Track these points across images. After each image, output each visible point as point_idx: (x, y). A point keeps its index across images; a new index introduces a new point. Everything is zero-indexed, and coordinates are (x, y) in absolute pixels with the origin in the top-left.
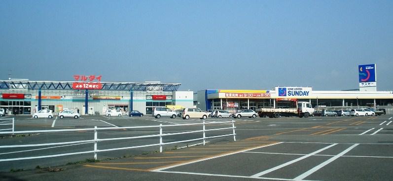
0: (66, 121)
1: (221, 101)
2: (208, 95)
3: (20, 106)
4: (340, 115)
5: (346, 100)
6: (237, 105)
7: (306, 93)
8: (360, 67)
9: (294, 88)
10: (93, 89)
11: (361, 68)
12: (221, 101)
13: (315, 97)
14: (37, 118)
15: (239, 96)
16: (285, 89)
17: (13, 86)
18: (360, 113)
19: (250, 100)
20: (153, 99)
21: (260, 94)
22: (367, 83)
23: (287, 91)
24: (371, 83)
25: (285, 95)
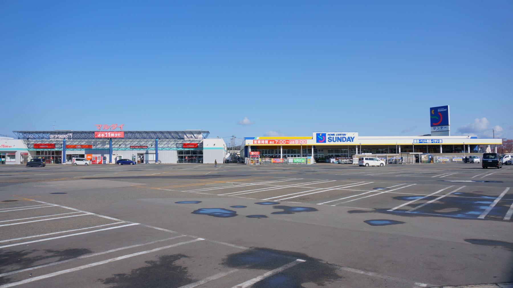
1: (441, 148)
3: (184, 155)
5: (444, 146)
6: (257, 153)
7: (351, 139)
8: (431, 109)
9: (336, 133)
10: (115, 138)
11: (433, 111)
12: (441, 148)
14: (369, 166)
15: (269, 143)
16: (324, 135)
17: (192, 135)
18: (371, 163)
19: (284, 147)
20: (183, 148)
21: (295, 141)
22: (440, 127)
23: (327, 137)
24: (444, 127)
25: (325, 142)
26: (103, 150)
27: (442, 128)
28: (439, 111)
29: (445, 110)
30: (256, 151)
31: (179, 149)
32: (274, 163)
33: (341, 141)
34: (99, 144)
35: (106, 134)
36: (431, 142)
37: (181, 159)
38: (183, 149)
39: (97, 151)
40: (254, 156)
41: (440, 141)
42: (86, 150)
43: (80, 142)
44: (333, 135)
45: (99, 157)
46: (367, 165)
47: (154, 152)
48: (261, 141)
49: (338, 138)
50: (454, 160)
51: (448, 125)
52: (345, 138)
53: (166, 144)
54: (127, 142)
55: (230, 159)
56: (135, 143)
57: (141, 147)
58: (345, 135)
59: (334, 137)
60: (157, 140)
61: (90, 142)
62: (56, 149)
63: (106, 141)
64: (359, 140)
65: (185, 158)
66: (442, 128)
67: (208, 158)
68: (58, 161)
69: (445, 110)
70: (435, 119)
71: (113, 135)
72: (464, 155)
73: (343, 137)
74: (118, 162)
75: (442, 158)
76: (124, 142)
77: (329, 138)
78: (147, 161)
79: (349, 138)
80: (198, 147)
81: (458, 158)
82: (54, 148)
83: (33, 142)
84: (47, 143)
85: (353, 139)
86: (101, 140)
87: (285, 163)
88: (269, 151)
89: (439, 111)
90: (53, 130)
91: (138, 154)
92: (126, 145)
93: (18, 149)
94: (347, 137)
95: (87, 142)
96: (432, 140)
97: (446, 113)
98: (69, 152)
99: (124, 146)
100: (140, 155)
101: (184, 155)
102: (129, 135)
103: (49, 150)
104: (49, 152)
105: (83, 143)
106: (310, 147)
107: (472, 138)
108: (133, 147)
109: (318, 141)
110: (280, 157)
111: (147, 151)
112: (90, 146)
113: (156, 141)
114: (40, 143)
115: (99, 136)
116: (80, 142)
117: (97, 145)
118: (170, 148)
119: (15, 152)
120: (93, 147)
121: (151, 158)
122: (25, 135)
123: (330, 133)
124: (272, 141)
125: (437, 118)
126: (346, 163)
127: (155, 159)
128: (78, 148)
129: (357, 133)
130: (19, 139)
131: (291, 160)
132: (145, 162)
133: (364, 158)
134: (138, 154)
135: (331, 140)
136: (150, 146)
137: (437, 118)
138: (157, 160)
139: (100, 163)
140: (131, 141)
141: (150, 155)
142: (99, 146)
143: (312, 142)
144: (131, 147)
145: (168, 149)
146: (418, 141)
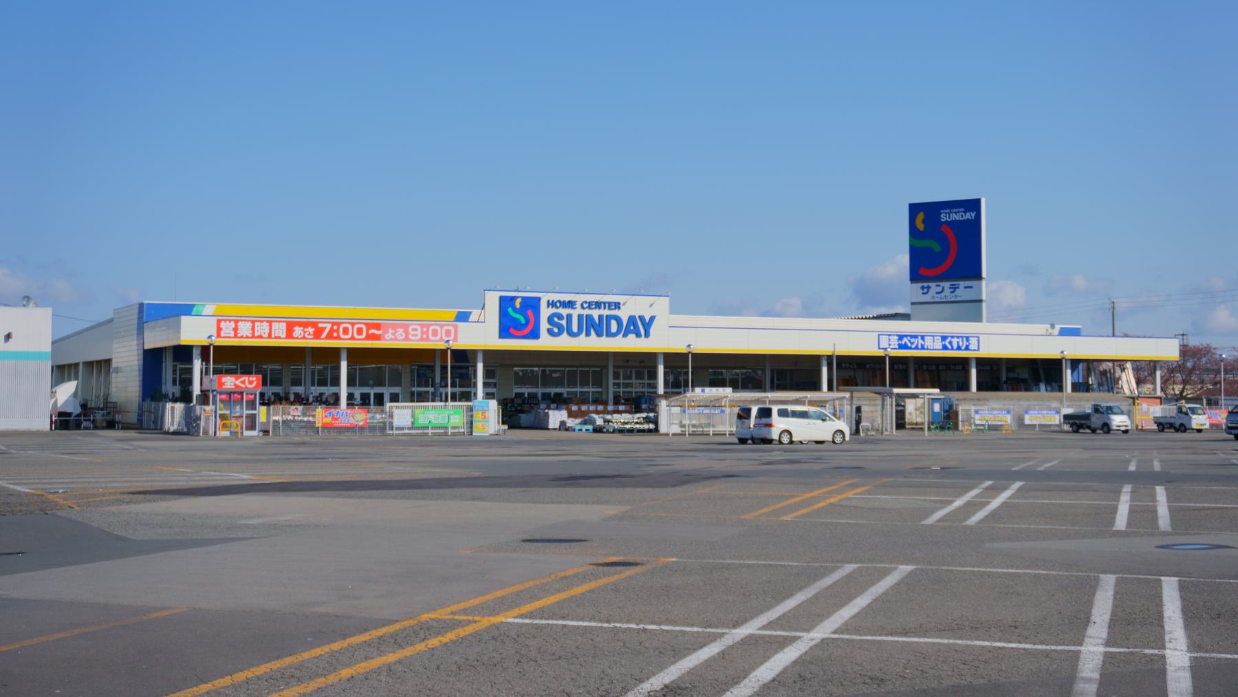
0: (344, 437)
1: (974, 372)
2: (913, 401)
4: (1183, 428)
6: (250, 383)
8: (914, 209)
11: (921, 216)
12: (974, 372)
13: (678, 347)
15: (289, 335)
16: (531, 305)
18: (803, 430)
19: (354, 354)
21: (406, 328)
22: (947, 285)
23: (545, 312)
24: (962, 284)
25: (535, 335)
27: (954, 288)
28: (944, 218)
29: (970, 216)
30: (246, 371)
32: (326, 427)
33: (599, 334)
36: (939, 345)
40: (233, 397)
41: (973, 342)
44: (570, 304)
46: (785, 439)
48: (264, 329)
49: (589, 317)
50: (1028, 420)
51: (978, 276)
52: (618, 320)
55: (75, 409)
58: (617, 306)
59: (575, 313)
64: (674, 334)
66: (954, 288)
68: (641, 402)
69: (970, 216)
70: (929, 249)
72: (1068, 402)
73: (609, 318)
75: (985, 411)
77: (550, 320)
79: (632, 320)
81: (1045, 410)
85: (647, 325)
87: (372, 429)
88: (288, 372)
89: (944, 218)
94: (624, 314)
96: (944, 338)
97: (974, 227)
106: (463, 358)
107: (1064, 332)
109: (504, 332)
110: (336, 400)
123: (555, 297)
124: (305, 325)
125: (937, 248)
126: (631, 431)
129: (664, 302)
131: (402, 415)
133: (775, 409)
135: (560, 328)
137: (937, 248)
143: (481, 334)
146: (895, 341)
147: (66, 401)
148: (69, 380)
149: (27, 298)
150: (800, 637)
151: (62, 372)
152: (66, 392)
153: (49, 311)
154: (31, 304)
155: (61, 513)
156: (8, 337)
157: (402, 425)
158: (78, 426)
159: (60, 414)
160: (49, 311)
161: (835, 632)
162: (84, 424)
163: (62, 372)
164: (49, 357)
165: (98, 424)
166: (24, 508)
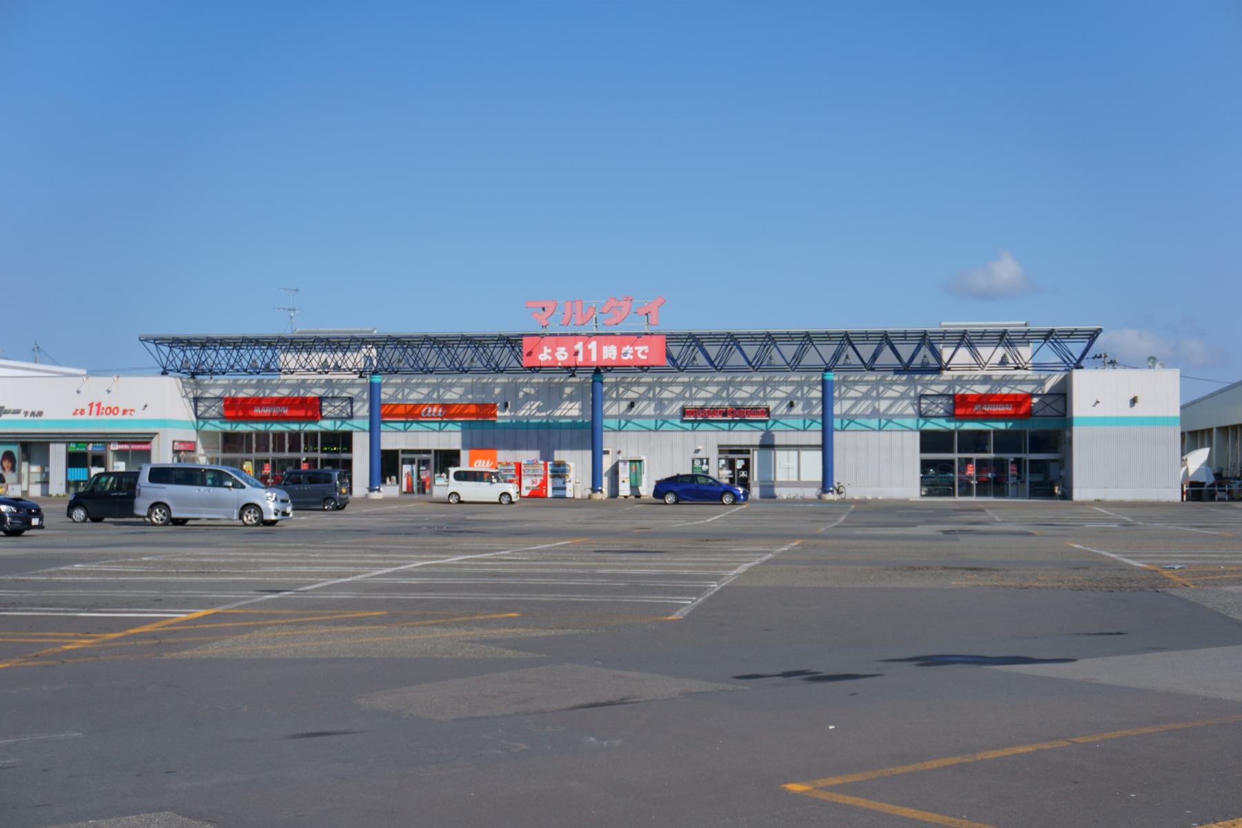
3: (955, 456)
20: (951, 416)
26: (547, 426)
31: (930, 426)
34: (528, 397)
35: (579, 346)
37: (936, 476)
38: (952, 426)
39: (519, 435)
42: (466, 427)
43: (435, 387)
45: (533, 463)
47: (817, 439)
53: (866, 396)
54: (664, 386)
55: (1208, 479)
56: (707, 394)
57: (738, 414)
60: (830, 376)
61: (486, 388)
62: (326, 425)
63: (561, 386)
65: (963, 469)
67: (1094, 475)
71: (610, 353)
74: (661, 489)
76: (650, 386)
78: (768, 493)
80: (1029, 414)
82: (316, 417)
83: (217, 387)
84: (284, 392)
86: (538, 379)
90: (287, 333)
91: (724, 450)
92: (661, 404)
93: (164, 423)
95: (470, 389)
98: (393, 439)
99: (650, 410)
100: (730, 453)
101: (955, 456)
102: (689, 352)
103: (295, 427)
104: (295, 436)
105: (452, 396)
108: (696, 411)
111: (768, 435)
112: (486, 410)
113: (824, 383)
114: (249, 393)
115: (544, 357)
116: (435, 387)
117: (517, 407)
118: (885, 421)
119: (147, 439)
120: (502, 416)
121: (795, 470)
122: (189, 355)
127: (818, 477)
128: (431, 419)
130: (165, 373)
132: (755, 492)
134: (724, 450)
136: (783, 410)
138: (827, 482)
139: (537, 494)
140: (687, 385)
141: (781, 455)
142: (530, 411)
144: (684, 412)
145: (874, 423)
147: (1199, 470)
148: (1203, 446)
149: (1153, 359)
150: (243, 487)
151: (1192, 438)
152: (1198, 459)
153: (1177, 372)
154: (1157, 366)
155: (1173, 592)
156: (1134, 401)
157: (58, 446)
158: (1212, 497)
159: (1192, 484)
160: (1177, 372)
161: (243, 487)
162: (1219, 495)
163: (1192, 438)
164: (1178, 422)
165: (1235, 495)
166: (1134, 585)
